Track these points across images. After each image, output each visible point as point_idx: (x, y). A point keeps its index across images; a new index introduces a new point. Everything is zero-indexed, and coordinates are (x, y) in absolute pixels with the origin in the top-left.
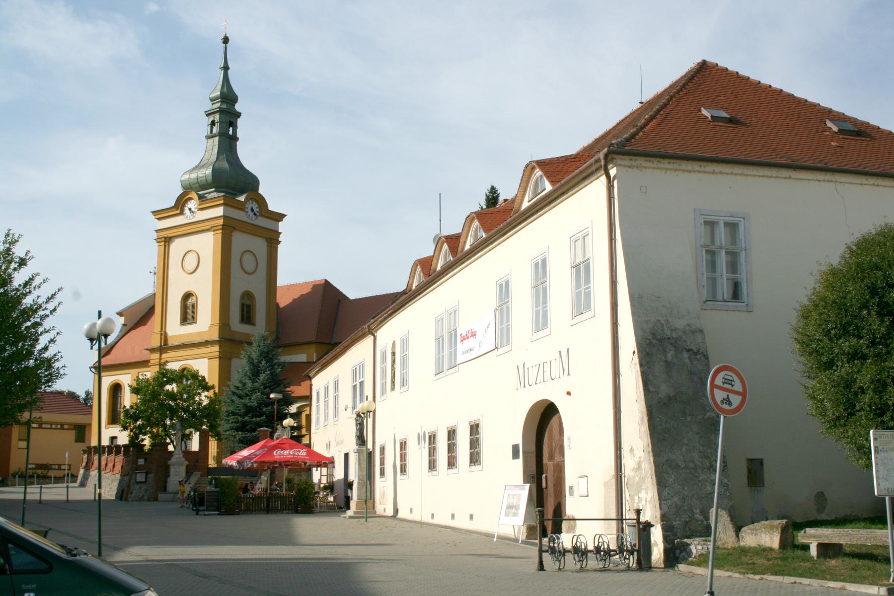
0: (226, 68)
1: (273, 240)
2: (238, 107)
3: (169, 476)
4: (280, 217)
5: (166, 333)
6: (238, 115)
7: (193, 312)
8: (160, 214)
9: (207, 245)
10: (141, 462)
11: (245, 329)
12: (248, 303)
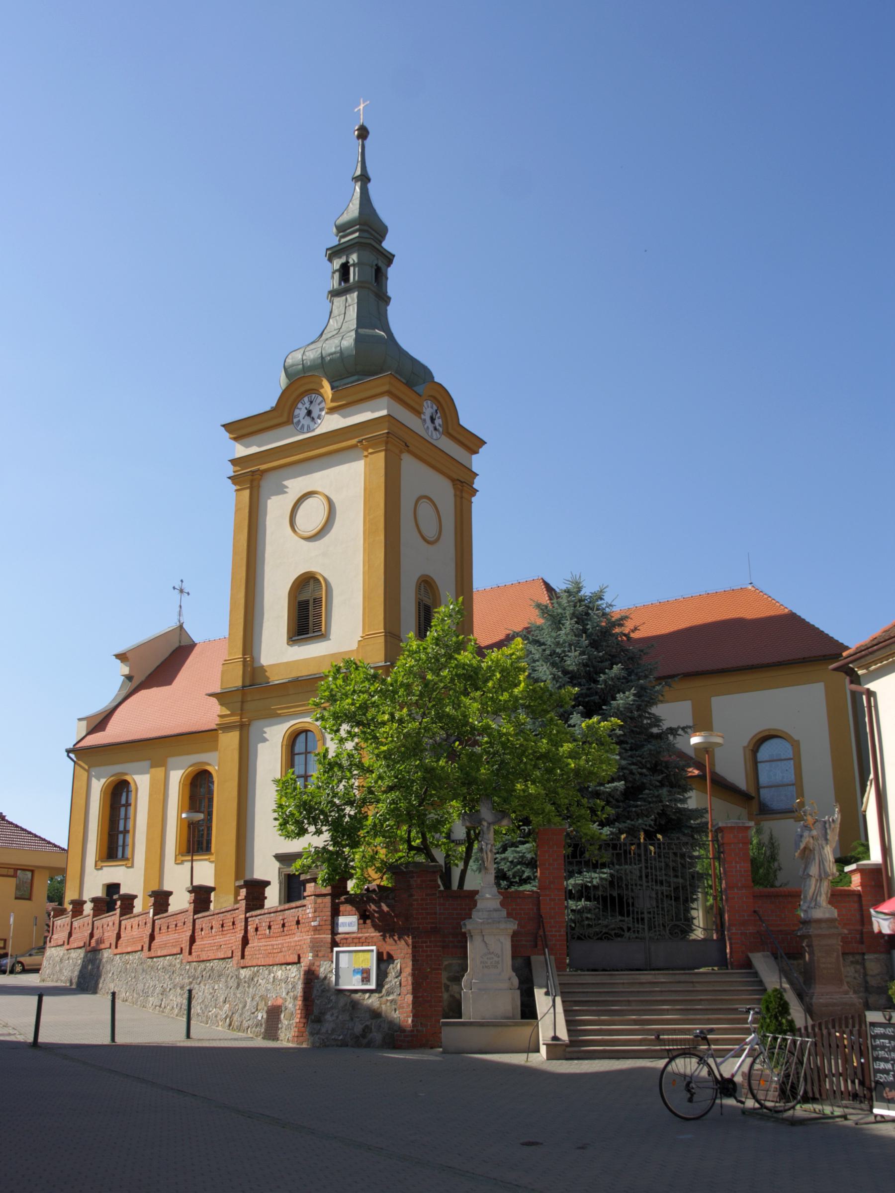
0: (364, 179)
1: (464, 485)
2: (388, 244)
4: (473, 443)
6: (389, 259)
8: (240, 430)
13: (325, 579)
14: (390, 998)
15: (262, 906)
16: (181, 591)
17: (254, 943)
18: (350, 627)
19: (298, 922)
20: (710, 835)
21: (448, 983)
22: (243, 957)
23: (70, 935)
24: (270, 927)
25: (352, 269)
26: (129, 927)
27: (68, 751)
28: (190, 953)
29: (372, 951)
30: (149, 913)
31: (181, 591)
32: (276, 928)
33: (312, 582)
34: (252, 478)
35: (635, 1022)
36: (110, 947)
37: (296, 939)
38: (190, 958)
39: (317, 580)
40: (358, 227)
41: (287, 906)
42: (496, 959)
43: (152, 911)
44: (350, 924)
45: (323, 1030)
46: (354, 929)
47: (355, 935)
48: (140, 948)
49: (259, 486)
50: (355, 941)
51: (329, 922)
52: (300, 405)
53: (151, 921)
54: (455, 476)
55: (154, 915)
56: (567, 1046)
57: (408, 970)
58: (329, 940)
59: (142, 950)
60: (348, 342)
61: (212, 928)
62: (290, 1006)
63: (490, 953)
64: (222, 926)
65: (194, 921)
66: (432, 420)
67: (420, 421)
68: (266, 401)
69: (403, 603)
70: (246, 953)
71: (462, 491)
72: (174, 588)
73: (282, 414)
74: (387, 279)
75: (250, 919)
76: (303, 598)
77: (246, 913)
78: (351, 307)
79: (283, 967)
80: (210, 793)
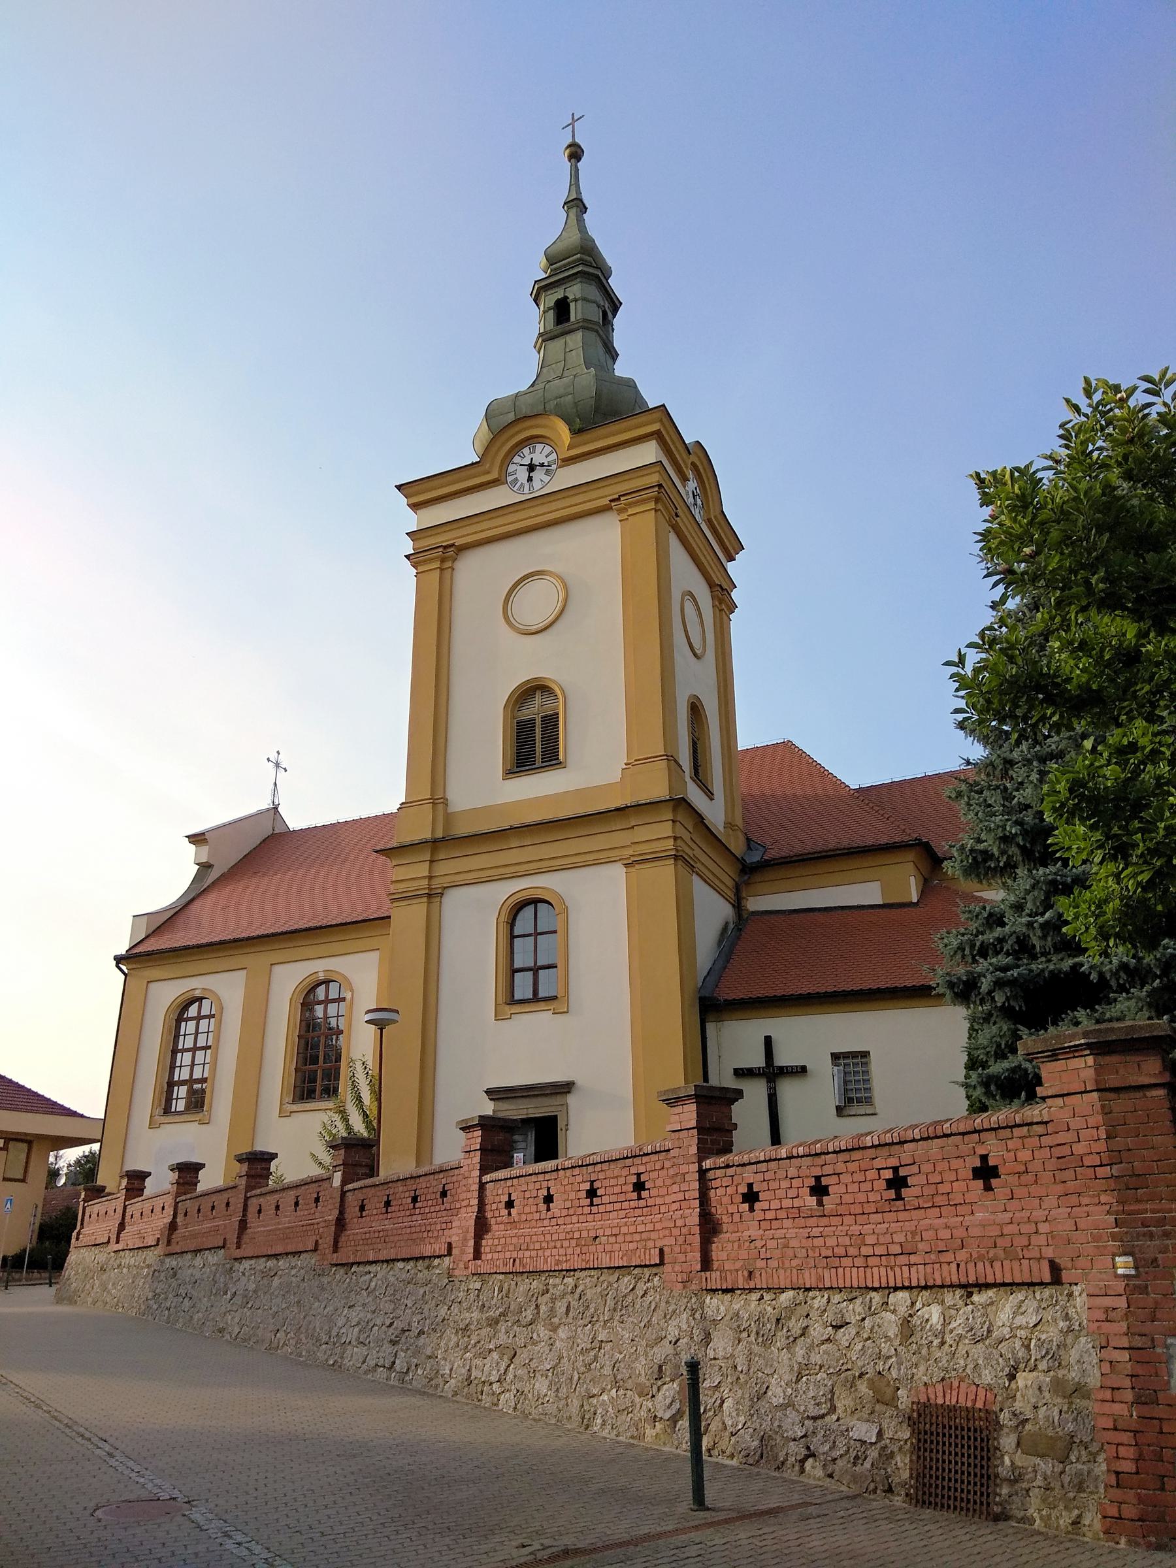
5: (446, 803)
8: (419, 493)
13: (562, 690)
16: (277, 765)
20: (1005, 1064)
22: (477, 1255)
23: (122, 1226)
25: (572, 305)
26: (94, 1216)
27: (119, 960)
30: (329, 1179)
31: (277, 765)
33: (538, 695)
34: (436, 555)
48: (311, 1246)
52: (526, 451)
53: (338, 1195)
55: (344, 1182)
65: (482, 1186)
72: (268, 760)
76: (526, 714)
77: (700, 1160)
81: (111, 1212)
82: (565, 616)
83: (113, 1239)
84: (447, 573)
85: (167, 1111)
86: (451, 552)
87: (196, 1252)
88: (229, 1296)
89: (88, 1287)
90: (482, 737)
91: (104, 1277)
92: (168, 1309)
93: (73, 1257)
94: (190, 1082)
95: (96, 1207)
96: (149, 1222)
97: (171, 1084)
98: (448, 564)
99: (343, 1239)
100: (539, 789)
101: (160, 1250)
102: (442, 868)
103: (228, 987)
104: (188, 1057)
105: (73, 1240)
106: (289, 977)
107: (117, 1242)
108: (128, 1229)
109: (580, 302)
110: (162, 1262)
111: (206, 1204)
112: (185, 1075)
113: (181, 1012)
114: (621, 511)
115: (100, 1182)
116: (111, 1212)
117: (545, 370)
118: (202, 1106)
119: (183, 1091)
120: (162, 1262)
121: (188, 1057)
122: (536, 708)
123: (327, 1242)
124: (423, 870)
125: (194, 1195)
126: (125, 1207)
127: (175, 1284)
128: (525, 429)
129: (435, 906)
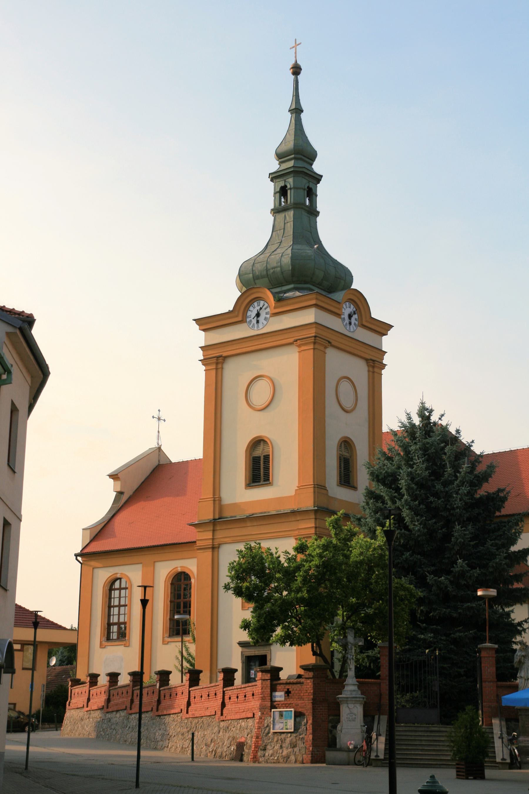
0: (297, 111)
1: (375, 362)
2: (317, 167)
3: (339, 721)
4: (382, 328)
5: (220, 499)
6: (318, 178)
7: (340, 465)
8: (206, 323)
9: (286, 367)
10: (279, 696)
11: (342, 494)
12: (346, 454)
14: (301, 737)
15: (232, 685)
16: (159, 419)
17: (228, 707)
18: (288, 482)
19: (253, 695)
21: (332, 729)
22: (222, 714)
23: (89, 700)
24: (237, 697)
25: (289, 192)
26: (76, 694)
27: (76, 555)
28: (187, 712)
29: (292, 711)
30: (156, 685)
31: (159, 419)
32: (241, 697)
33: (262, 443)
34: (215, 360)
35: (422, 750)
36: (126, 709)
37: (252, 704)
38: (188, 716)
39: (264, 441)
40: (293, 156)
41: (247, 685)
42: (354, 716)
43: (158, 684)
44: (281, 696)
45: (267, 754)
46: (283, 699)
47: (283, 703)
48: (150, 709)
49: (222, 368)
50: (283, 705)
51: (269, 695)
52: (251, 308)
53: (158, 691)
54: (369, 357)
55: (160, 687)
56: (383, 760)
57: (310, 722)
58: (269, 705)
59: (152, 710)
60: (287, 260)
61: (201, 697)
62: (249, 742)
63: (351, 713)
64: (208, 696)
65: (189, 692)
66: (350, 316)
67: (340, 320)
68: (228, 305)
69: (328, 461)
70: (224, 712)
71: (374, 372)
73: (237, 315)
74: (316, 196)
75: (226, 692)
77: (223, 688)
78: (289, 224)
79: (245, 720)
80: (190, 593)
81: (83, 693)
82: (272, 405)
83: (85, 706)
84: (220, 371)
85: (108, 639)
86: (220, 360)
87: (117, 711)
88: (127, 728)
89: (76, 728)
90: (236, 467)
91: (82, 723)
92: (108, 735)
93: (68, 714)
94: (119, 624)
95: (77, 690)
96: (99, 700)
97: (109, 625)
98: (220, 366)
99: (159, 707)
100: (261, 494)
101: (86, 709)
102: (219, 534)
103: (134, 574)
104: (116, 609)
105: (67, 706)
106: (164, 570)
107: (87, 707)
108: (92, 701)
109: (292, 191)
110: (105, 716)
111: (120, 691)
112: (116, 620)
113: (111, 586)
114: (299, 346)
115: (78, 677)
116: (83, 693)
117: (274, 233)
118: (125, 637)
119: (115, 628)
120: (105, 716)
121: (116, 609)
122: (259, 452)
123: (155, 708)
124: (209, 535)
125: (117, 687)
126: (89, 691)
127: (110, 724)
128: (252, 294)
129: (216, 553)
